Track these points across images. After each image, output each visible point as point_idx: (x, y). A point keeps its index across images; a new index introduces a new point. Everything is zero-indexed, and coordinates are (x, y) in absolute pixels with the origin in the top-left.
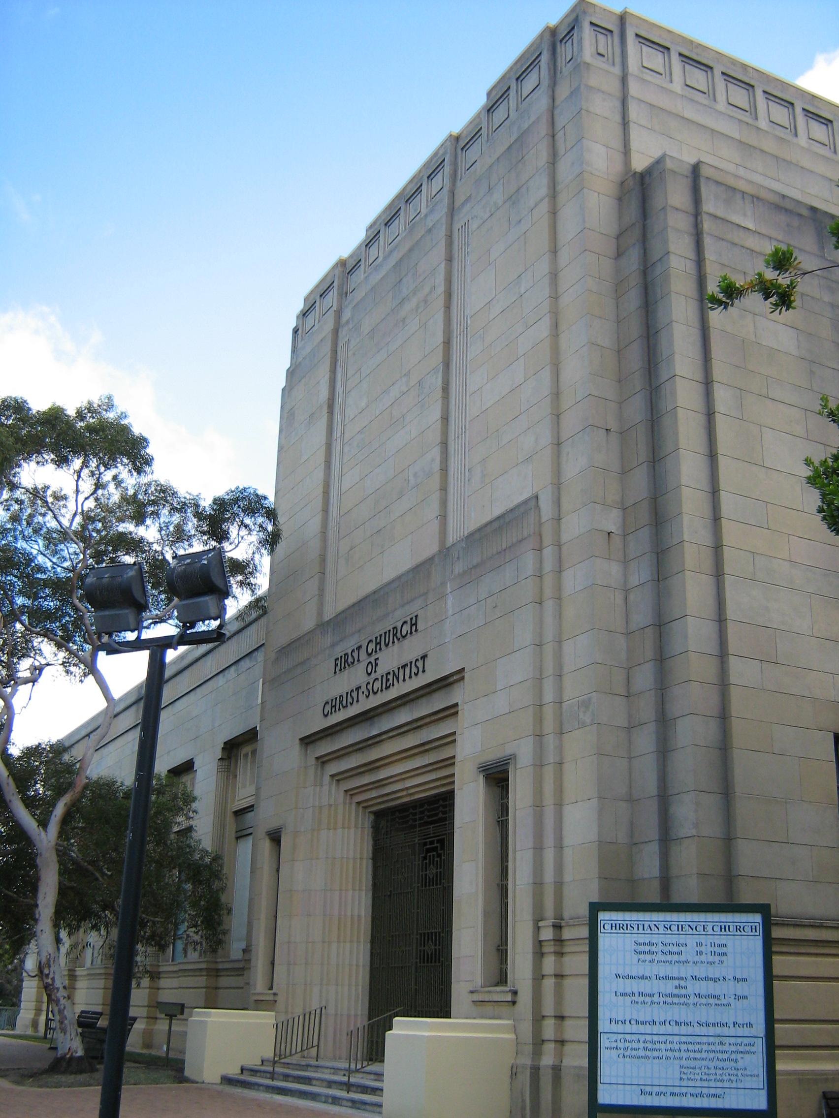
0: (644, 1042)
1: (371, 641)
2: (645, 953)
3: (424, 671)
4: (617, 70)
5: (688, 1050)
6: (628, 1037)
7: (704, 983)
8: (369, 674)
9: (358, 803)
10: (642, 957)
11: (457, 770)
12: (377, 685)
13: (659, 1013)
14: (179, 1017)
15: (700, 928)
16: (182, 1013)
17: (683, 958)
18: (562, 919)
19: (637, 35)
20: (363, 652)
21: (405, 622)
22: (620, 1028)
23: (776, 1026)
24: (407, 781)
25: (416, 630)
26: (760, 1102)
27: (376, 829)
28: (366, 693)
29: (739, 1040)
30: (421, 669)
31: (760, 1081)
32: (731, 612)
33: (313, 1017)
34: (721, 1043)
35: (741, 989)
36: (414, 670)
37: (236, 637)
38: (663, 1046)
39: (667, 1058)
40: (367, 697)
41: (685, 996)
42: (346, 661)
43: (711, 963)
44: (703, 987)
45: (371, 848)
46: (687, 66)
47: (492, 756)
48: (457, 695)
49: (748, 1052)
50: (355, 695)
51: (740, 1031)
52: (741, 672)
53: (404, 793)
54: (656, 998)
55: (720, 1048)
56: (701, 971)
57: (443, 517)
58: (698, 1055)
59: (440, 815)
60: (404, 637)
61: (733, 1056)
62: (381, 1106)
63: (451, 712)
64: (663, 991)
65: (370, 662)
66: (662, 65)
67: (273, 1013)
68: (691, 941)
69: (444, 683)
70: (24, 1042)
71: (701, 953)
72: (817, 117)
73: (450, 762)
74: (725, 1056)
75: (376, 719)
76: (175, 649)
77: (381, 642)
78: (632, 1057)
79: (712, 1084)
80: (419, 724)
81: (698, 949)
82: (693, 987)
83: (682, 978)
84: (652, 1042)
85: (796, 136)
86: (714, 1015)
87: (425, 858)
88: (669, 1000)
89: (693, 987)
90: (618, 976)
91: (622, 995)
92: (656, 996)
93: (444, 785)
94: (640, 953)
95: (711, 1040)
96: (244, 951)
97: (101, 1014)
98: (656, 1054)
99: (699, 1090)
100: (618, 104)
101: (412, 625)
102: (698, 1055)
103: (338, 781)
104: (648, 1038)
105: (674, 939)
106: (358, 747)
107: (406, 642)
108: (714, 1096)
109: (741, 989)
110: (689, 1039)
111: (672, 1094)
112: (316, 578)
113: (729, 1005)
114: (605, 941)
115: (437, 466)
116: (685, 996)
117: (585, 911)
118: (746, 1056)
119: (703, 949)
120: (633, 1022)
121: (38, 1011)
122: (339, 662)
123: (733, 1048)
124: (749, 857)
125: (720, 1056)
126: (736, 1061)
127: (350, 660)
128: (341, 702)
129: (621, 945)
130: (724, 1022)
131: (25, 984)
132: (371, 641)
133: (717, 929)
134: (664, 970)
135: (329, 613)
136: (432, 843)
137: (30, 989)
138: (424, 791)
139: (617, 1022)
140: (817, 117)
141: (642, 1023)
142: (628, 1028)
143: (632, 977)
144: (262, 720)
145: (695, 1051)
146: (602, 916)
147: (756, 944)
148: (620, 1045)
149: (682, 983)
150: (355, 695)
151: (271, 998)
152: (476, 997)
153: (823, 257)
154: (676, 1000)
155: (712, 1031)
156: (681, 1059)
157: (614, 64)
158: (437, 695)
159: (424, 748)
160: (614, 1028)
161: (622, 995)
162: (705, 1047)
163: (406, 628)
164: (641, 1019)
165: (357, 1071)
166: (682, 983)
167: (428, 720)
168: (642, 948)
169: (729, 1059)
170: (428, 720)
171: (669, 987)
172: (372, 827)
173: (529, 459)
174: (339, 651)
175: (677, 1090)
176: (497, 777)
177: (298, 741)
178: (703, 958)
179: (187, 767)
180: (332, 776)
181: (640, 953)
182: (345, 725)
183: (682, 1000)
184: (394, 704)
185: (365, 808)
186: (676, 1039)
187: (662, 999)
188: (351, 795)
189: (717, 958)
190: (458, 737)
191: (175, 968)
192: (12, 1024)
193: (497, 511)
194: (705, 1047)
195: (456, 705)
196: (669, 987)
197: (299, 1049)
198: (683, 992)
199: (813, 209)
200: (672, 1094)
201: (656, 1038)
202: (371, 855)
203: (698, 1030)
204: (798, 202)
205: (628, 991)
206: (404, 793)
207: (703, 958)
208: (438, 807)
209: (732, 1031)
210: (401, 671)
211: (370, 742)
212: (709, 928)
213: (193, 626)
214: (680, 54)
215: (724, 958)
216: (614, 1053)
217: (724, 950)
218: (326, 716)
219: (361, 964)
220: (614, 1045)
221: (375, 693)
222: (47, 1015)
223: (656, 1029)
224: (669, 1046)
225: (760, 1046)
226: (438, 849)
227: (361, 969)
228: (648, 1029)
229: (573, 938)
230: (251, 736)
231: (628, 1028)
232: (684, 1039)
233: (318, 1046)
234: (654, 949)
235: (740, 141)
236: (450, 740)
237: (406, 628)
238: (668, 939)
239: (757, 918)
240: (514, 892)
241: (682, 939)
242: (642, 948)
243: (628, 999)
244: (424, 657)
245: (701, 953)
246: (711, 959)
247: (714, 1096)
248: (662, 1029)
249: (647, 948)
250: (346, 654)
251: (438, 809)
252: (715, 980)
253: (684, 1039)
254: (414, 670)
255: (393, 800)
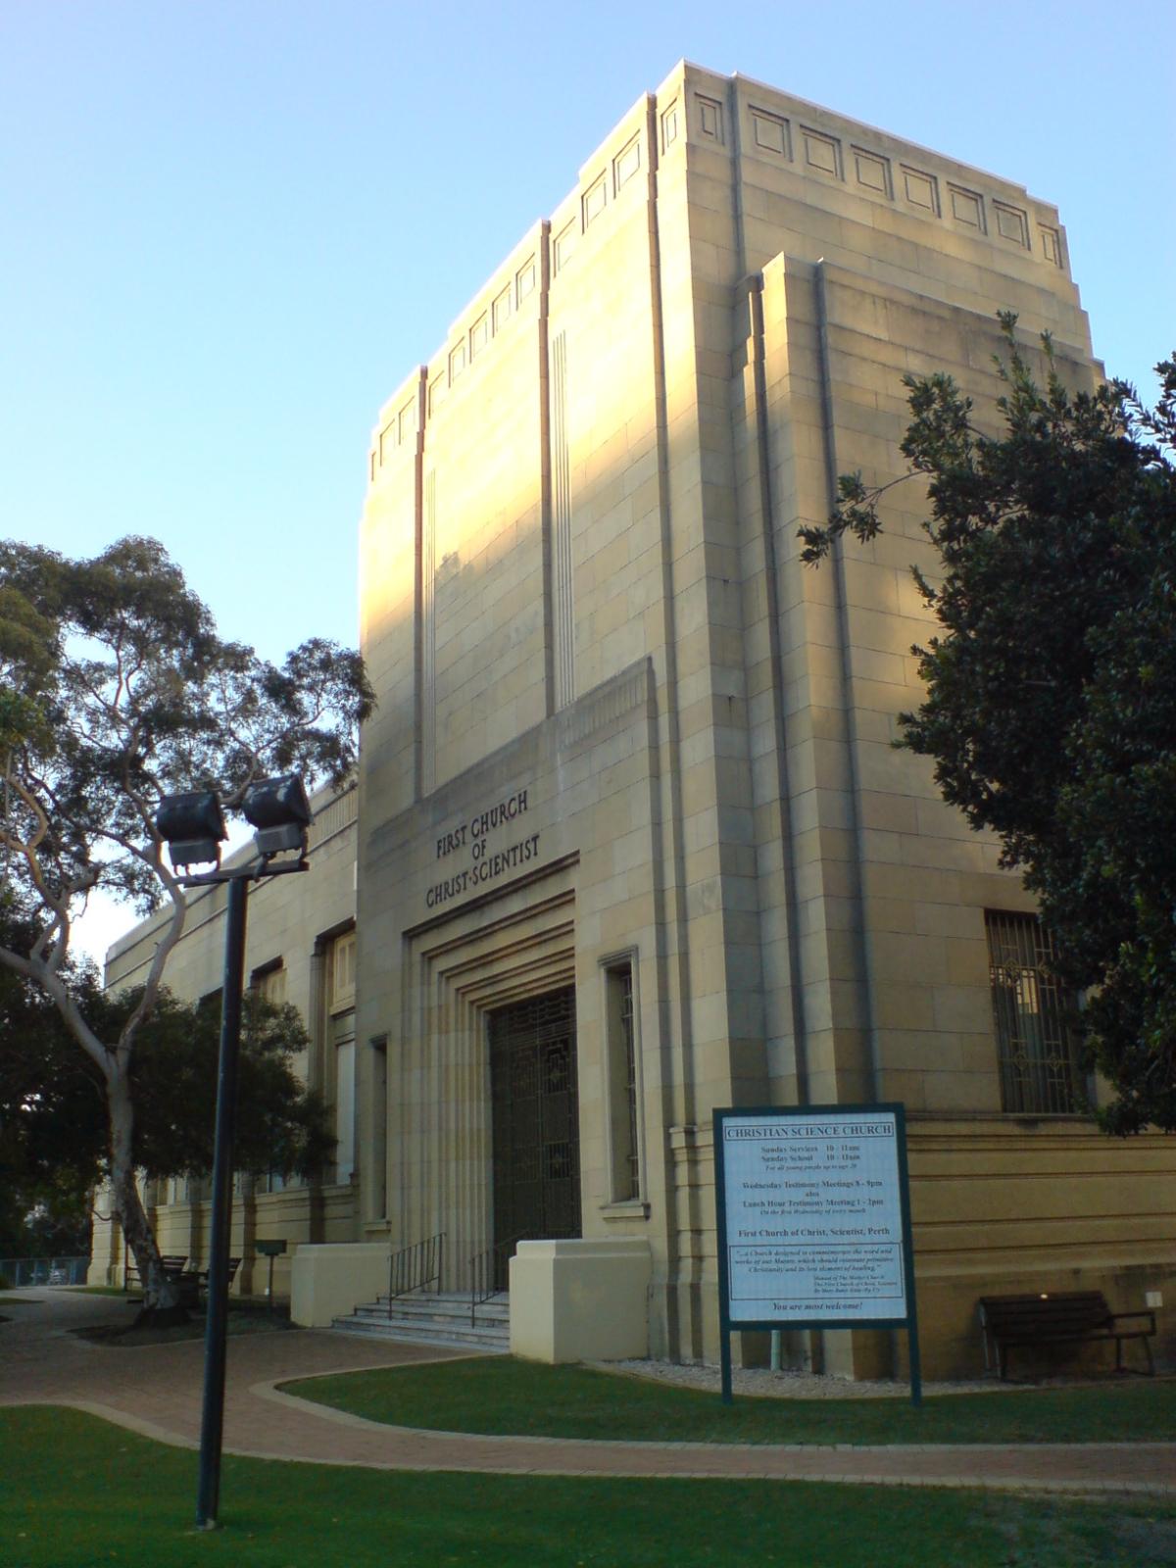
0: (777, 1254)
1: (476, 820)
2: (773, 1159)
3: (536, 854)
4: (726, 151)
5: (822, 1261)
6: (759, 1250)
7: (836, 1189)
8: (476, 858)
9: (472, 1003)
10: (770, 1164)
11: (577, 962)
12: (486, 870)
13: (790, 1223)
14: (281, 1255)
15: (830, 1131)
16: (284, 1251)
17: (813, 1163)
18: (694, 1124)
19: (750, 106)
20: (468, 832)
21: (513, 799)
22: (750, 1240)
23: (913, 1230)
24: (522, 974)
25: (526, 808)
26: (899, 1311)
27: (493, 1031)
28: (474, 879)
29: (876, 1248)
30: (533, 852)
31: (899, 1290)
32: (865, 780)
33: (432, 1244)
34: (857, 1252)
35: (875, 1193)
36: (525, 852)
37: (324, 813)
38: (796, 1258)
39: (801, 1269)
40: (475, 883)
41: (817, 1203)
42: (450, 843)
43: (843, 1167)
44: (837, 1194)
45: (488, 1052)
46: (810, 140)
47: (613, 946)
48: (573, 880)
49: (886, 1260)
50: (461, 881)
51: (876, 1238)
52: (877, 847)
53: (522, 989)
54: (787, 1208)
55: (856, 1256)
56: (833, 1176)
57: (550, 679)
58: (833, 1265)
59: (563, 1012)
60: (513, 816)
61: (870, 1265)
62: (508, 1338)
63: (567, 899)
64: (794, 1200)
65: (477, 845)
66: (780, 141)
67: (388, 1244)
68: (822, 1145)
69: (559, 867)
70: (100, 1296)
71: (833, 1157)
72: (966, 193)
73: (569, 954)
74: (861, 1265)
75: (486, 909)
76: (257, 881)
77: (488, 822)
78: (763, 1270)
79: (849, 1294)
80: (534, 912)
81: (830, 1153)
82: (827, 1194)
83: (812, 1185)
84: (785, 1254)
85: (940, 216)
86: (849, 1222)
87: (548, 1061)
88: (801, 1208)
89: (827, 1194)
90: (745, 1186)
91: (750, 1205)
92: (787, 1204)
93: (564, 979)
94: (768, 1160)
95: (847, 1248)
96: (352, 1176)
97: (185, 1258)
98: (789, 1266)
99: (835, 1302)
100: (727, 192)
101: (520, 803)
102: (833, 1265)
103: (448, 978)
104: (781, 1249)
105: (803, 1144)
106: (467, 939)
107: (514, 821)
108: (850, 1306)
109: (875, 1193)
110: (824, 1249)
111: (807, 1307)
112: (413, 746)
113: (864, 1211)
114: (731, 1149)
115: (540, 621)
116: (817, 1203)
117: (710, 1116)
118: (883, 1264)
119: (834, 1153)
120: (764, 1233)
121: (114, 1259)
122: (442, 845)
123: (870, 1256)
124: (887, 1049)
125: (857, 1265)
126: (873, 1270)
127: (454, 842)
128: (447, 890)
129: (752, 1150)
130: (859, 1228)
131: (96, 1229)
132: (476, 820)
133: (848, 1131)
134: (794, 1177)
135: (428, 790)
136: (554, 1043)
137: (102, 1233)
138: (545, 985)
139: (747, 1234)
140: (966, 193)
141: (773, 1234)
142: (759, 1240)
143: (761, 1187)
144: (358, 912)
145: (830, 1261)
146: (727, 1122)
147: (892, 1145)
148: (750, 1258)
149: (814, 1190)
150: (461, 881)
151: (384, 1227)
152: (608, 1213)
153: (968, 367)
154: (808, 1208)
155: (846, 1239)
156: (815, 1270)
157: (723, 144)
158: (552, 880)
159: (540, 939)
160: (744, 1240)
161: (750, 1205)
162: (840, 1256)
163: (514, 806)
164: (770, 1230)
165: (482, 1302)
166: (814, 1190)
167: (543, 908)
168: (770, 1155)
169: (865, 1268)
170: (543, 908)
171: (799, 1195)
172: (489, 1028)
173: (641, 614)
174: (442, 831)
175: (812, 1303)
176: (619, 972)
177: (400, 936)
178: (835, 1162)
179: (276, 965)
180: (441, 973)
181: (768, 1160)
182: (451, 916)
183: (815, 1208)
184: (505, 891)
185: (479, 1007)
186: (809, 1249)
187: (793, 1208)
188: (463, 994)
189: (849, 1163)
190: (575, 926)
191: (274, 1199)
192: (82, 1278)
193: (608, 675)
194: (840, 1256)
195: (573, 891)
196: (799, 1195)
197: (418, 1283)
198: (815, 1199)
199: (956, 310)
200: (807, 1307)
201: (789, 1249)
202: (488, 1061)
203: (833, 1239)
204: (939, 304)
205: (757, 1201)
206: (522, 989)
207: (835, 1162)
208: (559, 1005)
209: (868, 1238)
210: (511, 854)
211: (481, 934)
212: (840, 1130)
213: (273, 855)
214: (802, 126)
215: (856, 1162)
216: (746, 1267)
217: (857, 1153)
218: (430, 906)
219: (483, 1183)
220: (744, 1258)
221: (484, 879)
222: (126, 1262)
223: (790, 1239)
224: (802, 1257)
225: (897, 1253)
226: (562, 1052)
227: (483, 1188)
228: (779, 1240)
229: (701, 1143)
230: (347, 927)
231: (759, 1240)
232: (817, 1249)
233: (440, 1278)
234: (782, 1155)
235: (873, 228)
236: (567, 930)
237: (514, 806)
238: (797, 1144)
239: (891, 1118)
240: (642, 1097)
241: (811, 1144)
242: (770, 1155)
243: (758, 1209)
244: (535, 838)
245: (833, 1157)
246: (843, 1163)
247: (850, 1306)
248: (794, 1240)
249: (775, 1155)
250: (450, 836)
251: (560, 1002)
252: (848, 1185)
253: (817, 1249)
254: (525, 852)
255: (512, 996)
